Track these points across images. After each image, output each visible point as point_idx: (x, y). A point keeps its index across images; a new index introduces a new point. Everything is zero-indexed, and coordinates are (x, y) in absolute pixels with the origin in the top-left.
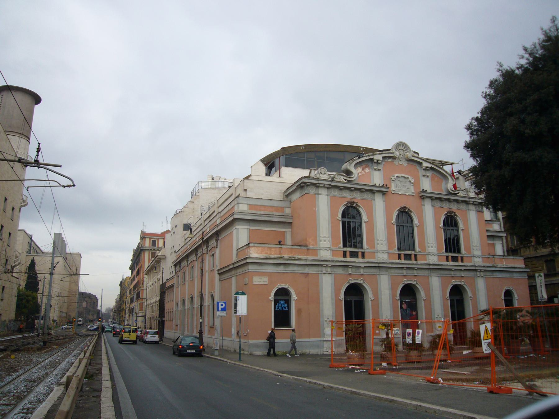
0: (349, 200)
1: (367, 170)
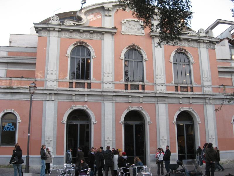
0: (78, 40)
1: (99, 17)
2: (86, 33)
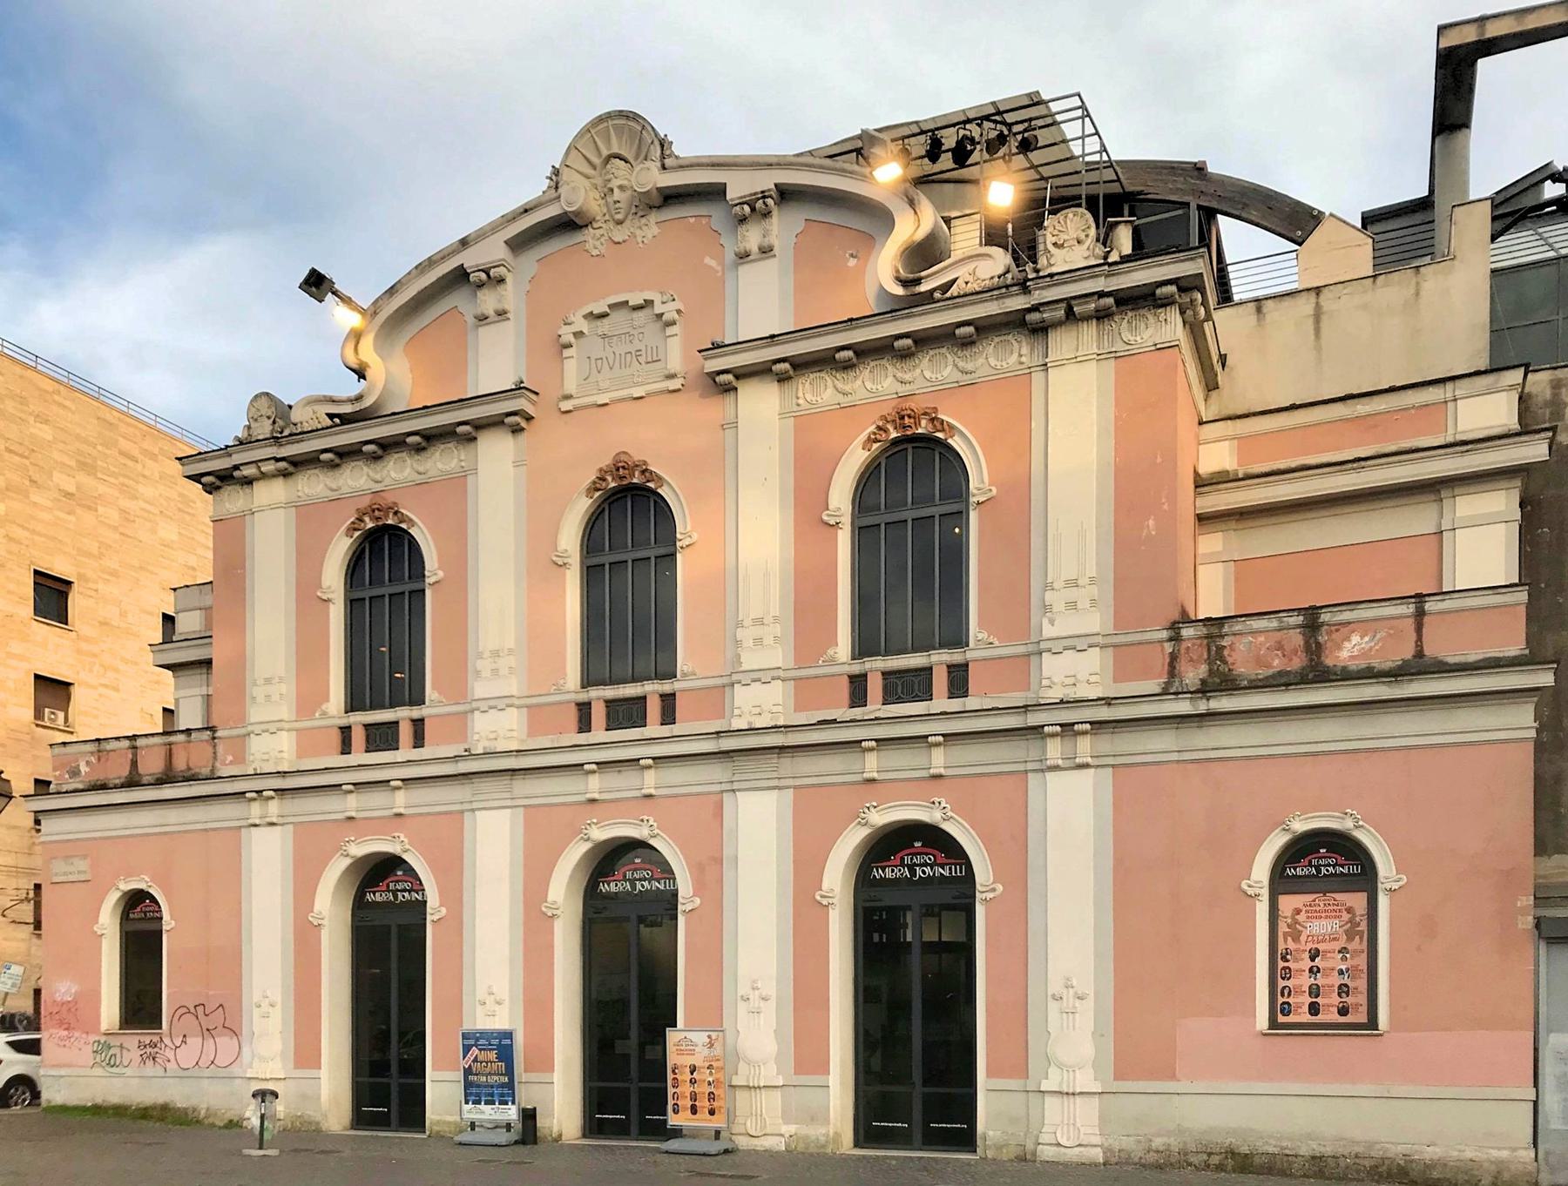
2: (997, 340)
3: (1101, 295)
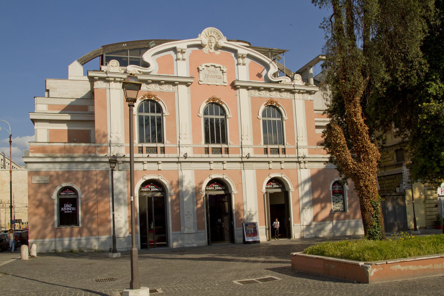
3: (121, 78)
